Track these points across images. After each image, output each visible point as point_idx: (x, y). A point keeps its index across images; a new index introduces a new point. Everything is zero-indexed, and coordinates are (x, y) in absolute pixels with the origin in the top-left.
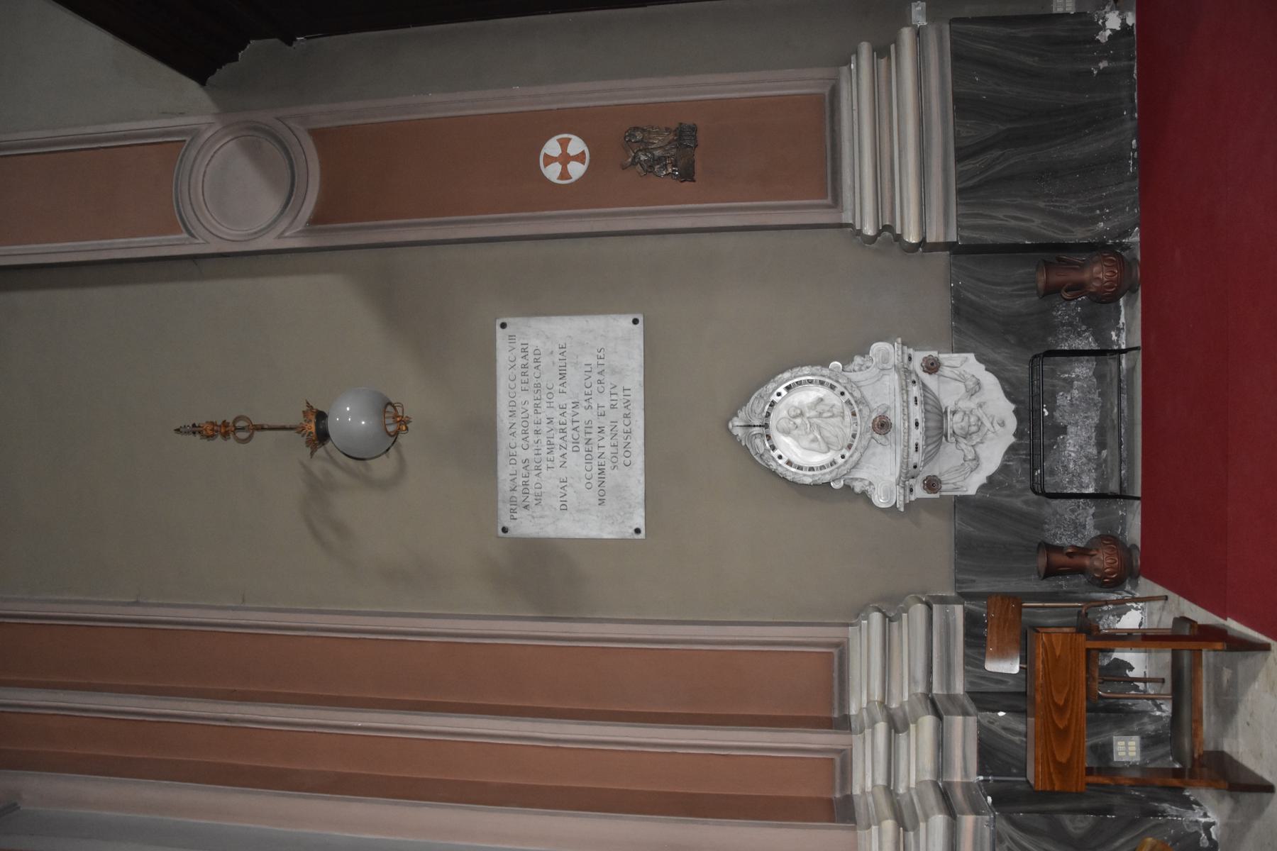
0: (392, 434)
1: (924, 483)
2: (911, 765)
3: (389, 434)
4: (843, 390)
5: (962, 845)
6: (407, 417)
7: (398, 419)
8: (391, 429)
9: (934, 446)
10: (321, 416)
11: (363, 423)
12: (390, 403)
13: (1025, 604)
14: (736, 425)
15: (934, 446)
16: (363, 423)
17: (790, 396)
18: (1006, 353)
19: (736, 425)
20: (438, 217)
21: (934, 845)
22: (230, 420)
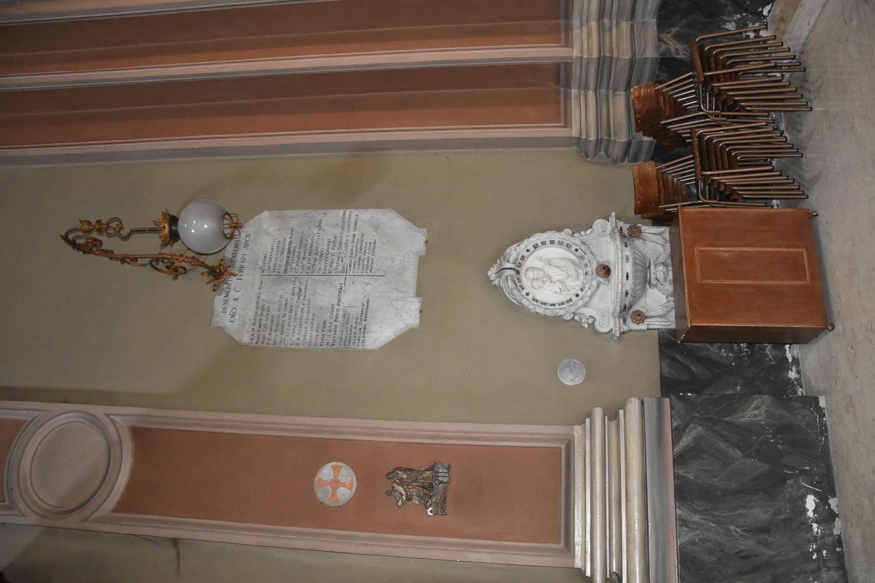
0: (228, 236)
1: (634, 322)
2: (584, 124)
3: (225, 235)
4: (580, 296)
5: (639, 434)
6: (240, 224)
7: (233, 225)
8: (228, 231)
9: (640, 291)
10: (173, 220)
11: (206, 226)
12: (227, 214)
13: (694, 178)
14: (492, 273)
15: (640, 291)
16: (206, 226)
17: (536, 251)
18: (713, 481)
19: (492, 273)
20: (328, 528)
21: (592, 42)
22: (104, 221)
